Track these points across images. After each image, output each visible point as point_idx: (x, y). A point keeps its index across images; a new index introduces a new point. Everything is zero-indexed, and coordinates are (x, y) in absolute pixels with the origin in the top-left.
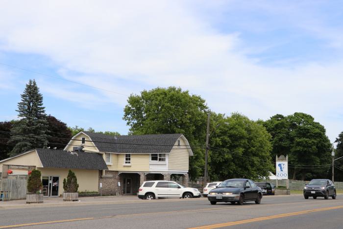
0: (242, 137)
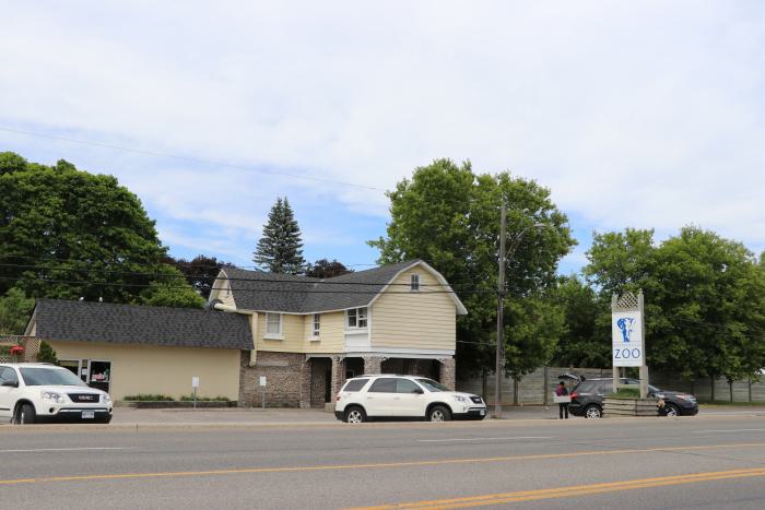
0: (704, 281)
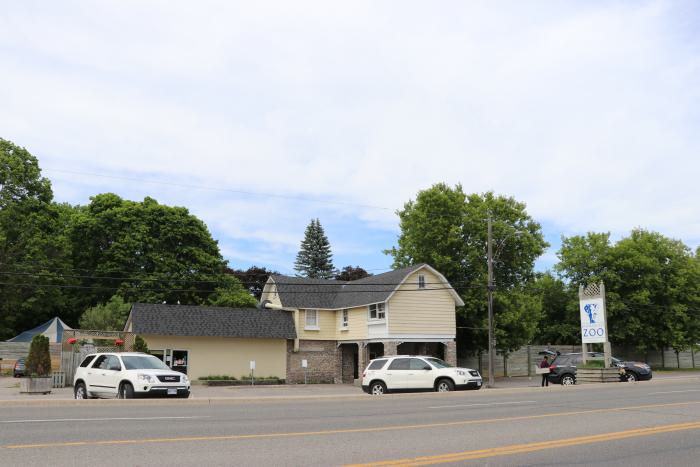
0: (647, 271)
